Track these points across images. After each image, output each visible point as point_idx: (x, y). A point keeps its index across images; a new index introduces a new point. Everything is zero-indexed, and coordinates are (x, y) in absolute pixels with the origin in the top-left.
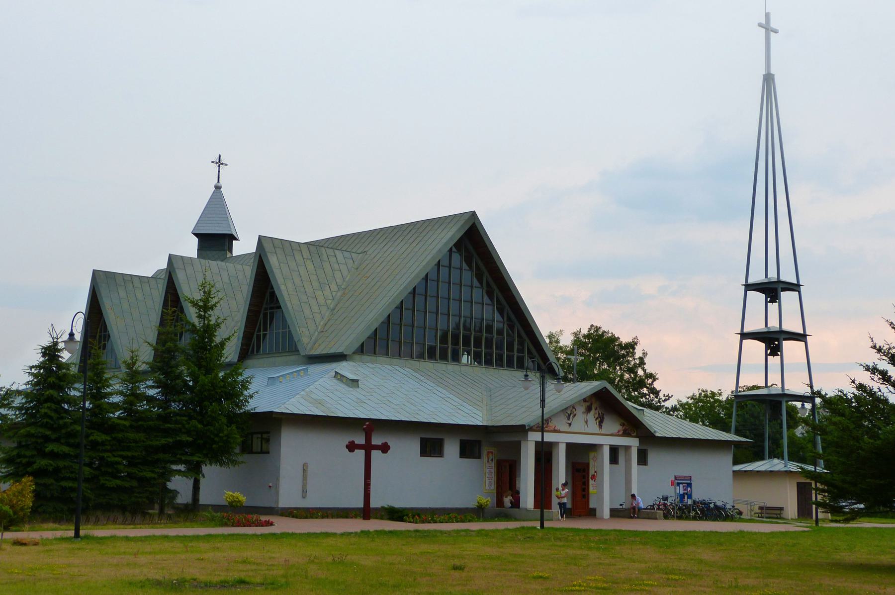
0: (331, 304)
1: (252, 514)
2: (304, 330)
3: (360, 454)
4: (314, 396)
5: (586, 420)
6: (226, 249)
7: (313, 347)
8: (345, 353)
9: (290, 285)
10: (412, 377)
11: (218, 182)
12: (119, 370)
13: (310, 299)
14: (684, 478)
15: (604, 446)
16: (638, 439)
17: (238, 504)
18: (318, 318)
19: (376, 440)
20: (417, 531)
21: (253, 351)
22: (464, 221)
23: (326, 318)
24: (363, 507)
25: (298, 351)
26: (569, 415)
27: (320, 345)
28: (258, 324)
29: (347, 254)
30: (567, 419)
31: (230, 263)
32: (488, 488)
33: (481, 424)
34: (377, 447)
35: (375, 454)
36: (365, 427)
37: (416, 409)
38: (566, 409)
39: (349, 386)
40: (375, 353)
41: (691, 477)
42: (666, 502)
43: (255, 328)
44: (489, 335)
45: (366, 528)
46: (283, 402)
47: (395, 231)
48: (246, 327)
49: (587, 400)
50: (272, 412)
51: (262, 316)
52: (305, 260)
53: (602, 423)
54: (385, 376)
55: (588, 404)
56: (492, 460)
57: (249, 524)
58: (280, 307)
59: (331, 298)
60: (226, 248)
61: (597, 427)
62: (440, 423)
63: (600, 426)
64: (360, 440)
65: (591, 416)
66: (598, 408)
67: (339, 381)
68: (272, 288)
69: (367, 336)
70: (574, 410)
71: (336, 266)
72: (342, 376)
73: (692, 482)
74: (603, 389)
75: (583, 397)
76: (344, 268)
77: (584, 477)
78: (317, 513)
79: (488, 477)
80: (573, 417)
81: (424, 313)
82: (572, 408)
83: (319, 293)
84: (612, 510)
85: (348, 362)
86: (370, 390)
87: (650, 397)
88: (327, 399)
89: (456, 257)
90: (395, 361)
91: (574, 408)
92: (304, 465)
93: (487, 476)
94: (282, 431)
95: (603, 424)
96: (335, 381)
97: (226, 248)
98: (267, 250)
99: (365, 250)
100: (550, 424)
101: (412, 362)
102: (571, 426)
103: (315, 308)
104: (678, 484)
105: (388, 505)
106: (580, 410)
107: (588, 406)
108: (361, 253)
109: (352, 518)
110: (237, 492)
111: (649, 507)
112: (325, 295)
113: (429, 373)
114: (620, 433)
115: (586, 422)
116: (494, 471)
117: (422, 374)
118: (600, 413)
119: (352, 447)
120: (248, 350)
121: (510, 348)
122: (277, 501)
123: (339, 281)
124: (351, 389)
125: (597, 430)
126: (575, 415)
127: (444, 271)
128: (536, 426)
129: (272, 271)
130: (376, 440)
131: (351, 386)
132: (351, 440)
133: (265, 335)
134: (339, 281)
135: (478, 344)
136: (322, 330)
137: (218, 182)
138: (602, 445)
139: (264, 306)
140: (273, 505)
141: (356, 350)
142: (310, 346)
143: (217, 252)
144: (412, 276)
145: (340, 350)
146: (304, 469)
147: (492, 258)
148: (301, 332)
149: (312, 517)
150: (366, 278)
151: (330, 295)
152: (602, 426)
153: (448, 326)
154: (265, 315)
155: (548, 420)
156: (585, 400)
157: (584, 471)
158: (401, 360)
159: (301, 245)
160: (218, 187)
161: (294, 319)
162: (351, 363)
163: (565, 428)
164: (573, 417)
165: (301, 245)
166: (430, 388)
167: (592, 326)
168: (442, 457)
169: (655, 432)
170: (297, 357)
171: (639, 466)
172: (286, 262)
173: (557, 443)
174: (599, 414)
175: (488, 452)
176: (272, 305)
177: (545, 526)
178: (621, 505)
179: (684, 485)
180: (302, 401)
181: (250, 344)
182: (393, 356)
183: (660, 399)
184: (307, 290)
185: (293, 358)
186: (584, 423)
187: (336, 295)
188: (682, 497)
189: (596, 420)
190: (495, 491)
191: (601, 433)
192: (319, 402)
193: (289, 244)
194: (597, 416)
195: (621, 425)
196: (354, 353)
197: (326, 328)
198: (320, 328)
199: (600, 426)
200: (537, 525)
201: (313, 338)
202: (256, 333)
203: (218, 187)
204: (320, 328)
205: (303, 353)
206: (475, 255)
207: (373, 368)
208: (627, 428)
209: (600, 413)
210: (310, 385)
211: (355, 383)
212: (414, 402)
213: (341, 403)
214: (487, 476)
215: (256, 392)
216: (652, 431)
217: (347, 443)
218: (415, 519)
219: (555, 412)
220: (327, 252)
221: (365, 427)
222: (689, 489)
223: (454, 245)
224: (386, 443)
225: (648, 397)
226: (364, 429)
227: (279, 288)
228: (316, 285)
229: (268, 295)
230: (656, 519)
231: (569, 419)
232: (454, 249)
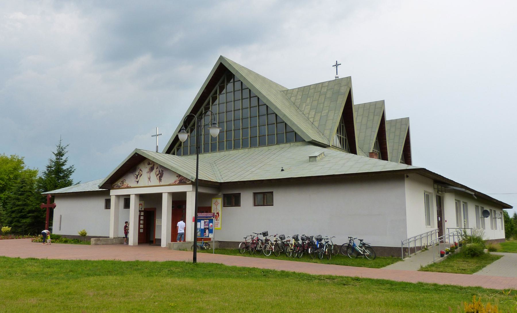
1: (177, 237)
5: (149, 177)
11: (337, 74)
16: (111, 190)
26: (137, 176)
30: (135, 178)
55: (151, 166)
61: (158, 181)
63: (160, 180)
70: (141, 171)
80: (140, 177)
82: (139, 171)
95: (162, 178)
100: (125, 184)
102: (139, 183)
107: (151, 167)
115: (149, 179)
118: (160, 170)
126: (141, 175)
137: (337, 74)
152: (161, 179)
163: (134, 184)
164: (140, 177)
174: (159, 171)
178: (446, 221)
179: (205, 221)
186: (148, 179)
189: (157, 176)
191: (161, 184)
194: (158, 173)
195: (177, 177)
199: (160, 180)
209: (160, 170)
231: (137, 178)
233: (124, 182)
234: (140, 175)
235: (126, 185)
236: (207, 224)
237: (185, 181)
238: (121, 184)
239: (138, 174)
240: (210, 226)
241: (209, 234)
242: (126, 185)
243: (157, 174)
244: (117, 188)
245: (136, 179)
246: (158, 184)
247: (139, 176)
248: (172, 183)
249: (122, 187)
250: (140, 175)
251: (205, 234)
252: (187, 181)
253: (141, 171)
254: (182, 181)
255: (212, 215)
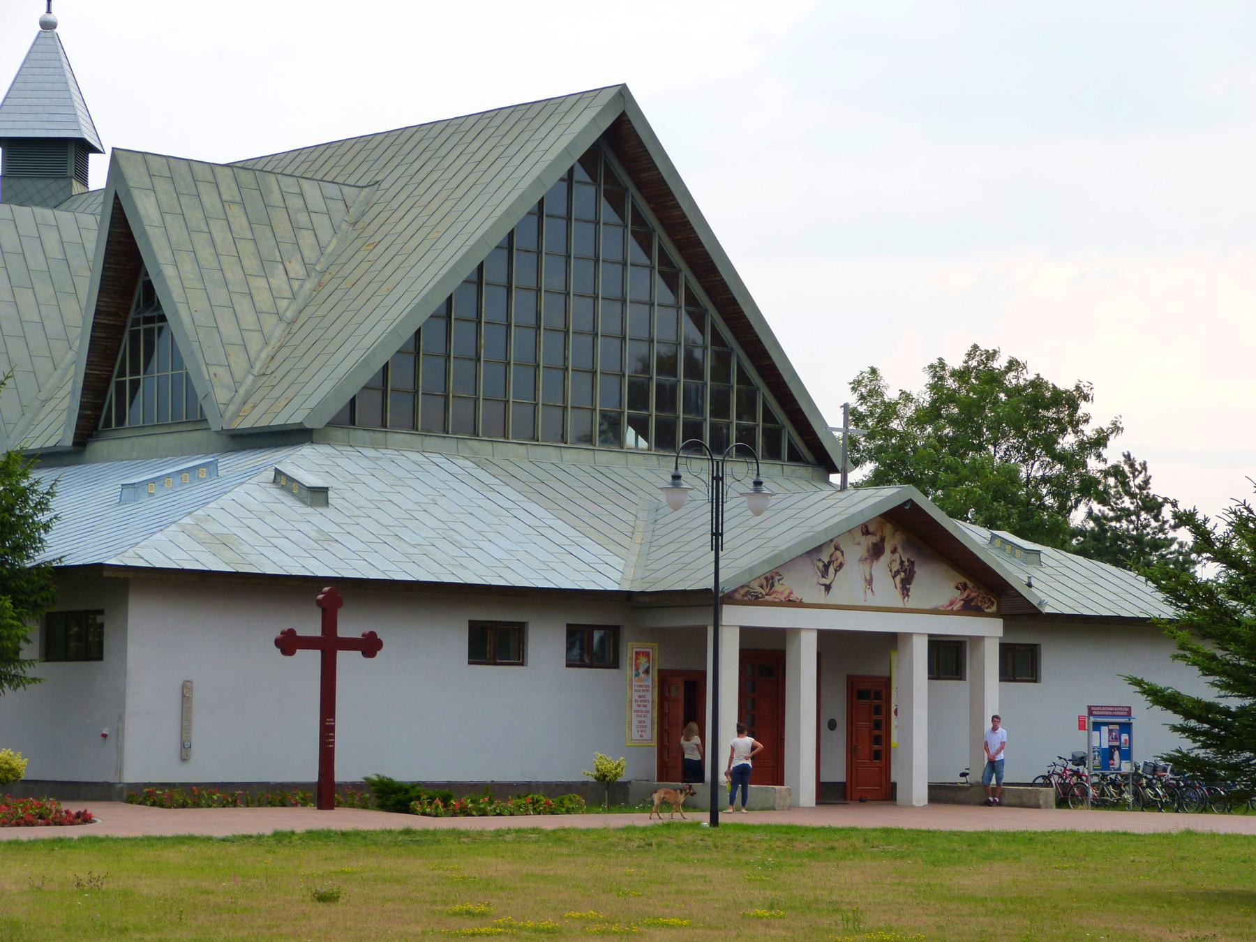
0: (287, 308)
2: (221, 371)
3: (310, 660)
4: (214, 528)
5: (868, 578)
6: (68, 174)
7: (239, 410)
8: (308, 426)
9: (187, 266)
10: (468, 479)
11: (49, 11)
12: (204, 426)
13: (235, 298)
14: (1113, 711)
15: (915, 638)
16: (1002, 620)
17: (10, 776)
18: (254, 341)
19: (348, 628)
20: (408, 832)
21: (108, 423)
22: (601, 107)
23: (274, 342)
24: (316, 779)
25: (206, 420)
26: (826, 567)
27: (254, 407)
28: (120, 356)
29: (332, 190)
31: (66, 210)
32: (636, 735)
33: (616, 587)
34: (350, 644)
35: (346, 660)
36: (320, 596)
37: (462, 554)
38: (818, 549)
39: (304, 502)
40: (384, 425)
41: (1130, 708)
42: (1081, 768)
43: (113, 367)
44: (694, 382)
45: (285, 826)
46: (131, 542)
47: (449, 131)
48: (89, 363)
49: (871, 529)
50: (99, 567)
51: (126, 338)
52: (226, 206)
53: (910, 584)
54: (400, 479)
55: (873, 539)
56: (647, 671)
57: (44, 819)
58: (163, 318)
59: (288, 294)
60: (71, 170)
61: (897, 593)
62: (514, 587)
63: (905, 591)
64: (311, 627)
65: (882, 570)
66: (899, 549)
67: (283, 492)
68: (147, 274)
69: (363, 385)
70: (838, 553)
71: (303, 218)
72: (290, 479)
73: (1132, 721)
74: (905, 504)
75: (862, 521)
76: (322, 223)
77: (878, 710)
78: (210, 795)
79: (635, 711)
81: (505, 328)
82: (832, 549)
83: (259, 283)
84: (932, 788)
85: (315, 446)
86: (357, 512)
87: (1138, 519)
88: (244, 534)
89: (585, 194)
90: (431, 442)
91: (837, 548)
92: (183, 687)
93: (635, 707)
94: (130, 606)
95: (913, 588)
96: (275, 492)
97: (71, 170)
98: (131, 184)
99: (377, 179)
100: (777, 587)
101: (475, 444)
103: (249, 320)
104: (1097, 726)
105: (378, 776)
106: (854, 553)
107: (874, 545)
108: (365, 187)
109: (295, 805)
110: (7, 749)
111: (1040, 781)
112: (273, 287)
113: (513, 470)
114: (957, 606)
115: (870, 582)
116: (652, 696)
117: (497, 471)
118: (905, 559)
119: (289, 643)
120: (99, 417)
121: (720, 408)
122: (120, 771)
123: (310, 254)
124: (310, 510)
125: (898, 601)
126: (841, 565)
127: (553, 229)
128: (742, 592)
129: (144, 233)
130: (348, 628)
131: (309, 501)
132: (286, 627)
133: (135, 385)
134: (310, 254)
135: (666, 398)
136: (263, 371)
137: (49, 11)
138: (911, 634)
139: (132, 314)
140: (110, 779)
141: (338, 415)
142: (232, 408)
143: (49, 181)
144: (471, 242)
145: (297, 419)
146: (183, 696)
147: (670, 194)
148: (212, 376)
149: (197, 805)
150: (372, 247)
151: (286, 287)
152: (908, 590)
153: (565, 359)
154: (135, 337)
155: (772, 578)
156: (865, 530)
157: (878, 695)
158: (447, 442)
159: (217, 169)
160: (48, 26)
161: (195, 345)
162: (324, 449)
165: (217, 169)
166: (508, 504)
167: (975, 347)
168: (522, 664)
169: (1041, 603)
170: (204, 433)
171: (1002, 683)
172: (179, 211)
173: (796, 631)
174: (902, 563)
175: (636, 653)
176: (148, 314)
177: (719, 821)
178: (963, 775)
179: (1111, 727)
180: (182, 539)
181: (102, 406)
182: (428, 431)
183: (1165, 522)
184: (229, 276)
185: (197, 436)
186: (863, 584)
187: (301, 287)
188: (1107, 755)
189: (894, 577)
190: (655, 744)
192: (223, 542)
193: (187, 169)
194: (896, 567)
195: (957, 588)
196: (330, 424)
197: (273, 366)
198: (258, 365)
199: (905, 591)
200: (705, 819)
201: (242, 391)
202: (114, 379)
203: (48, 26)
204: (258, 365)
205: (215, 427)
206: (632, 190)
207: (375, 459)
208: (974, 594)
210: (208, 503)
211: (321, 496)
212: (458, 538)
213: (281, 542)
214: (635, 707)
215: (56, 518)
216: (1035, 603)
217: (278, 634)
218: (434, 806)
219: (787, 558)
220: (281, 184)
221: (320, 596)
222: (1125, 737)
223: (580, 161)
224: (373, 634)
225: (1134, 518)
226: (319, 603)
227: (160, 273)
228: (251, 264)
229: (140, 287)
230: (1038, 806)
231: (825, 573)
232: (580, 174)
233: (776, 583)
234: (836, 564)
235: (782, 593)
236: (1116, 736)
237: (980, 604)
238: (762, 587)
239: (828, 559)
240: (1123, 740)
241: (1121, 762)
242: (782, 593)
243: (894, 570)
244: (746, 599)
245: (823, 577)
246: (898, 601)
247: (831, 566)
248: (942, 606)
249: (768, 598)
250: (836, 564)
251: (1111, 762)
252: (986, 605)
253: (838, 553)
254: (972, 604)
255: (1126, 713)
